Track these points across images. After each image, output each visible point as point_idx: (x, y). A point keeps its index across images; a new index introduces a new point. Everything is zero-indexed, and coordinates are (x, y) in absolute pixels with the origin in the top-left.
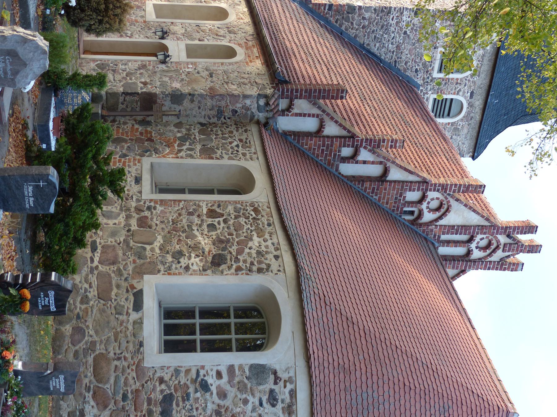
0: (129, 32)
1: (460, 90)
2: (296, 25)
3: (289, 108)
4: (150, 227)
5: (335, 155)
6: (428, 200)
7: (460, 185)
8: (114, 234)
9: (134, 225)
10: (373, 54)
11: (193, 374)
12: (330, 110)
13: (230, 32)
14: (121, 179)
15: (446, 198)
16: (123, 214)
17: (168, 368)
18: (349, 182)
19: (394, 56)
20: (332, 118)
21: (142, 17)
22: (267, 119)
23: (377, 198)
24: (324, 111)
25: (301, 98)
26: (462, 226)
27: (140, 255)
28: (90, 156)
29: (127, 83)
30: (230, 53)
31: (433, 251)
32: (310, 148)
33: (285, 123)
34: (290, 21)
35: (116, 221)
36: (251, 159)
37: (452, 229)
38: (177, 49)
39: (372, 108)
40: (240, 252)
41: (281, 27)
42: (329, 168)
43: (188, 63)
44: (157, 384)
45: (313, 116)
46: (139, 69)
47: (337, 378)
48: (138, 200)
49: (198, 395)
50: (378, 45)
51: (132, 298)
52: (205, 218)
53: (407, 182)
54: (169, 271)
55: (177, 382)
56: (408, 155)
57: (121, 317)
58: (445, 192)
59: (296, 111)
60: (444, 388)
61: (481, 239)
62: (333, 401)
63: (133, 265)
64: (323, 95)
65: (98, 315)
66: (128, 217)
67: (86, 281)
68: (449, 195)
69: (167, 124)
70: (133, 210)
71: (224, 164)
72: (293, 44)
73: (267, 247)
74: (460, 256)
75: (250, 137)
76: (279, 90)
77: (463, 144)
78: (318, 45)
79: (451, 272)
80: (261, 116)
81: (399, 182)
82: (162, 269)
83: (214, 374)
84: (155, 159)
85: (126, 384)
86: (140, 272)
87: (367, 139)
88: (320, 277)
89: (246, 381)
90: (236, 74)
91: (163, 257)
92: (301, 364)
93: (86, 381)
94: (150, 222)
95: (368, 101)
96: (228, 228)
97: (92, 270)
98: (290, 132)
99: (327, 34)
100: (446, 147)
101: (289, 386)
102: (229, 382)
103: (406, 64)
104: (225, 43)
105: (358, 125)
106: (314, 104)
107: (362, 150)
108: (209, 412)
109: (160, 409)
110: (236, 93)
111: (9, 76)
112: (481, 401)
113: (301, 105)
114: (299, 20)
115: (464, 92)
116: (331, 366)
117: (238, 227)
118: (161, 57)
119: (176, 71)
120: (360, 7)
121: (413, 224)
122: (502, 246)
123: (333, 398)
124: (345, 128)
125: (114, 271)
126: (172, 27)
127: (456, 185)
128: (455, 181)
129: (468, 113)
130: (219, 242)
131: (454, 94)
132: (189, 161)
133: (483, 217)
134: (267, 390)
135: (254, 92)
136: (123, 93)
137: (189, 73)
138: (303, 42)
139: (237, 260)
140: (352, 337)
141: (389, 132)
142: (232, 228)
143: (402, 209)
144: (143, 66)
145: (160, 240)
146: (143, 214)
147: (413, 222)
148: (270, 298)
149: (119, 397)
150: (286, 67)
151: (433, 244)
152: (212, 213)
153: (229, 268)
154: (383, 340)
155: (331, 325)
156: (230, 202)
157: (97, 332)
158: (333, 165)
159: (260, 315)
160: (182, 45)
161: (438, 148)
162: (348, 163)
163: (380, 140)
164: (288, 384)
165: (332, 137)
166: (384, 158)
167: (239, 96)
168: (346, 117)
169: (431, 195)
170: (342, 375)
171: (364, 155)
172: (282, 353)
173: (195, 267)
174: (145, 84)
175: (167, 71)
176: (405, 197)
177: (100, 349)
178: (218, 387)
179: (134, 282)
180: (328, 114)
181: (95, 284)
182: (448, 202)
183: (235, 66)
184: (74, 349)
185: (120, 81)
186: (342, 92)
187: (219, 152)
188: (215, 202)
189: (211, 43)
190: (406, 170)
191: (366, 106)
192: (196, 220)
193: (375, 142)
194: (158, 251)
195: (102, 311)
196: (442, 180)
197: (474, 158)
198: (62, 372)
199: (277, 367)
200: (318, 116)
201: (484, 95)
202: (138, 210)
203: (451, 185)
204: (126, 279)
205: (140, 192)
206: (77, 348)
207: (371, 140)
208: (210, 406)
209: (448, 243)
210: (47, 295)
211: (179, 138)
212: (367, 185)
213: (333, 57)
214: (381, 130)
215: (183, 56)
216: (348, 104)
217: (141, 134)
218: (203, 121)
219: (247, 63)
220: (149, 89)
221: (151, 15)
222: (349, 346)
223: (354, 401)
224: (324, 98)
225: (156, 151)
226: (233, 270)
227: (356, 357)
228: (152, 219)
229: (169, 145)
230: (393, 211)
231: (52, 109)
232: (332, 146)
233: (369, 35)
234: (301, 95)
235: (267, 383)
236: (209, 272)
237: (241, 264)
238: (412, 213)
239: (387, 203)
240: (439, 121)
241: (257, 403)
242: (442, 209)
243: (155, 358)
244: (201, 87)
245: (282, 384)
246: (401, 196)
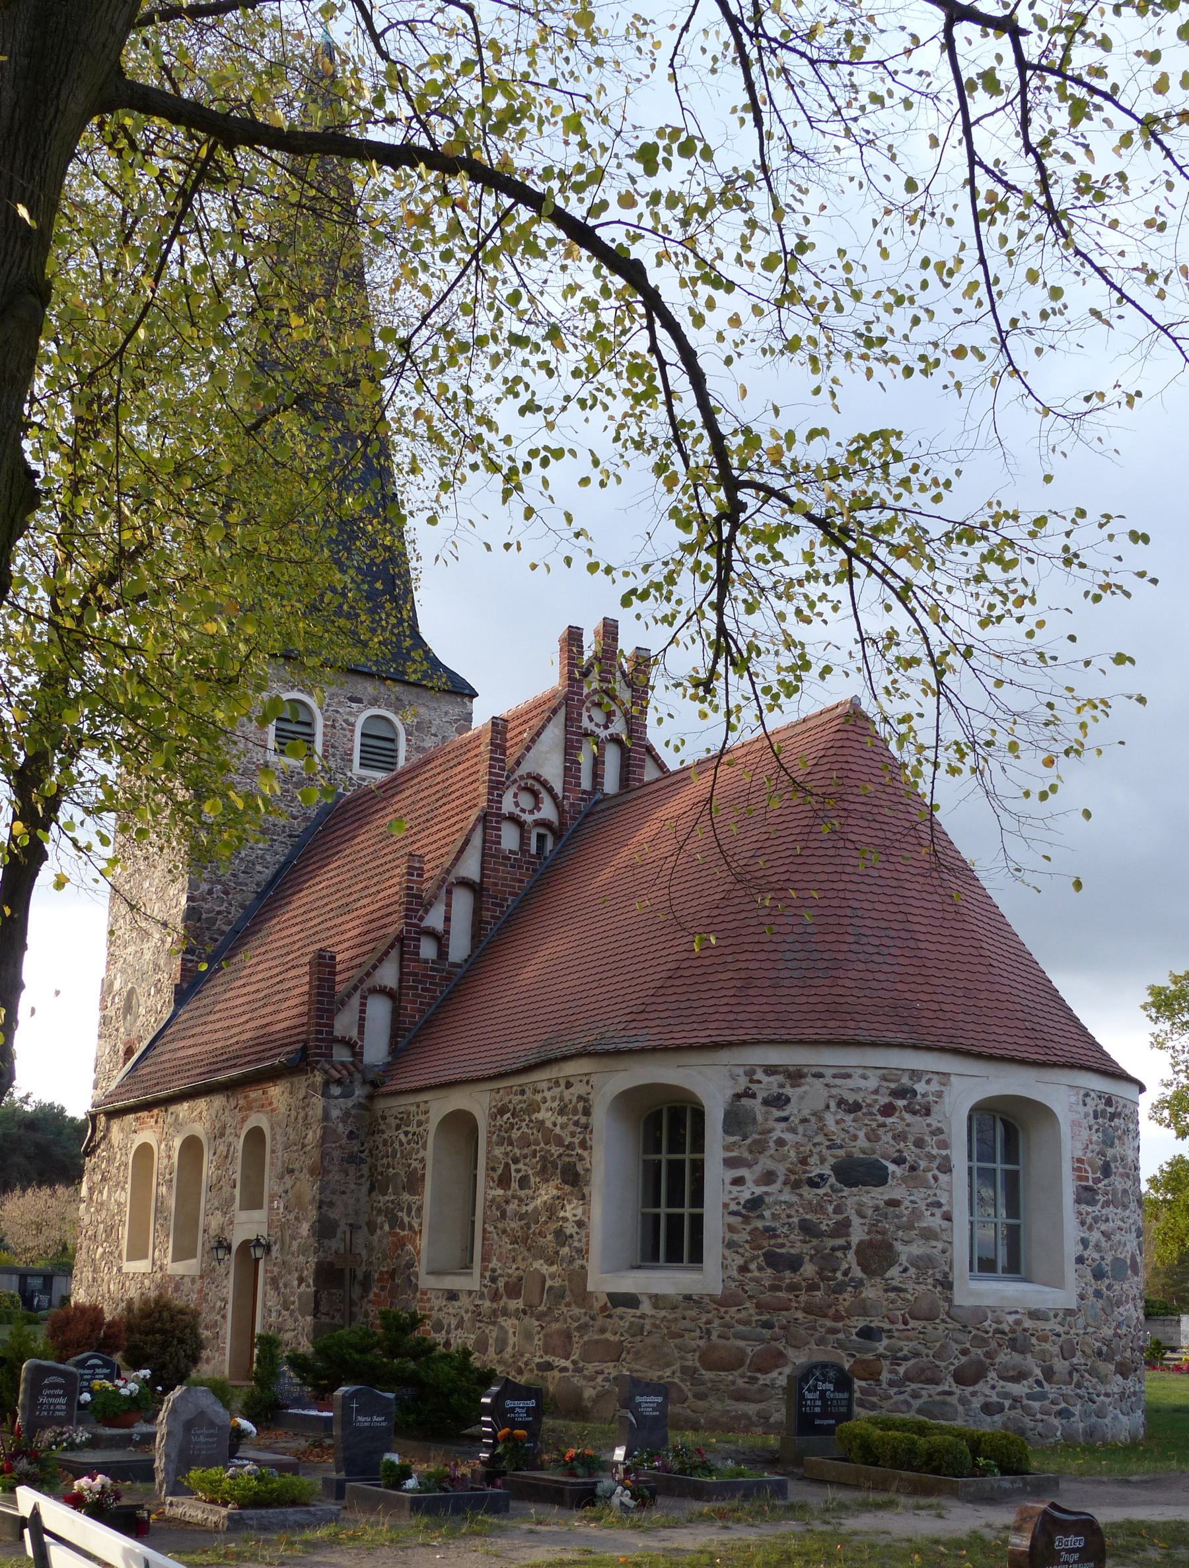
0: (219, 1304)
1: (346, 721)
2: (218, 1016)
3: (350, 1044)
4: (520, 1279)
5: (432, 969)
6: (517, 811)
7: (491, 759)
8: (528, 1336)
9: (517, 1304)
10: (276, 875)
11: (735, 1220)
12: (357, 973)
13: (222, 1135)
14: (397, 1317)
15: (515, 781)
16: (501, 1320)
17: (724, 1258)
18: (482, 946)
19: (281, 839)
20: (368, 974)
21: (193, 1281)
22: (364, 1082)
23: (510, 898)
24: (355, 988)
25: (332, 1026)
26: (566, 754)
27: (558, 1295)
28: (356, 1356)
29: (299, 1309)
30: (256, 1135)
31: (613, 803)
32: (419, 1010)
33: (376, 1050)
34: (210, 1027)
35: (511, 1331)
36: (426, 1112)
37: (571, 770)
38: (248, 1225)
39: (364, 893)
40: (559, 1141)
41: (219, 1045)
42: (455, 979)
43: (271, 1209)
44: (749, 1275)
45: (363, 1005)
46: (277, 1288)
47: (755, 1000)
48: (482, 1296)
49: (767, 1214)
50: (259, 868)
51: (620, 1310)
52: (510, 1193)
53: (484, 849)
54: (583, 1253)
55: (747, 1246)
56: (435, 847)
57: (647, 1327)
58: (503, 783)
59: (354, 1034)
60: (796, 823)
61: (591, 719)
62: (788, 1008)
63: (573, 1306)
64: (326, 987)
65: (643, 1361)
66: (505, 1312)
67: (592, 1379)
68: (508, 778)
69: (369, 1247)
70: (495, 1306)
71: (430, 1155)
72: (248, 1026)
73: (553, 1099)
74: (622, 755)
75: (394, 1111)
76: (318, 1062)
77: (446, 713)
78: (254, 979)
79: (650, 773)
80: (360, 1092)
81: (483, 862)
82: (580, 1262)
83: (736, 1188)
84: (421, 1268)
85: (746, 1323)
86: (583, 1297)
87: (406, 916)
88: (604, 1017)
89: (749, 1141)
90: (289, 1130)
91: (562, 1260)
92: (724, 1056)
93: (740, 1382)
94: (514, 1279)
95: (340, 909)
96: (525, 1157)
97: (578, 1370)
98: (391, 1044)
99: (235, 960)
100: (440, 761)
101: (759, 1075)
102: (749, 1166)
103: (295, 818)
104: (239, 1144)
105: (385, 926)
106: (343, 1003)
107: (426, 923)
108: (795, 1199)
109: (788, 1273)
110: (319, 1133)
111: (215, 1431)
112: (825, 760)
113: (344, 1024)
114: (208, 1010)
115: (350, 713)
116: (736, 1009)
117: (525, 1142)
118: (259, 1253)
119: (282, 1227)
120: (189, 899)
121: (561, 836)
122: (605, 686)
123: (784, 1008)
124: (386, 953)
125: (581, 1337)
126: (212, 1232)
127: (491, 766)
128: (483, 767)
129: (388, 705)
130: (545, 1172)
131: (352, 731)
132: (426, 1212)
133: (549, 719)
134: (764, 1109)
135: (318, 1102)
136: (315, 1316)
137: (286, 1208)
138: (246, 1008)
139: (570, 1146)
140: (698, 971)
141: (396, 880)
142: (525, 1151)
143: (532, 856)
144: (274, 1282)
145: (538, 1264)
146: (501, 1290)
147: (557, 836)
148: (630, 1100)
149: (767, 1333)
150: (282, 1046)
151: (596, 803)
152: (504, 1181)
153: (581, 1159)
154: (709, 921)
155: (675, 1006)
156: (489, 1152)
157: (668, 1365)
158: (449, 973)
159: (657, 1115)
160: (242, 1216)
161: (439, 778)
162: (447, 946)
163: (408, 895)
164: (755, 1077)
165: (402, 973)
166: (439, 887)
167: (324, 1128)
168: (371, 946)
169: (508, 805)
170: (752, 992)
171: (434, 919)
172: (710, 1083)
173: (579, 1211)
174: (301, 1280)
175: (283, 1243)
176: (511, 852)
177: (692, 1361)
178: (758, 1183)
179: (597, 1305)
180: (361, 981)
181: (597, 1366)
182: (521, 777)
183: (278, 1130)
184: (691, 1399)
185: (296, 1321)
186: (323, 957)
187: (415, 1164)
188: (487, 1176)
189: (239, 1168)
190: (462, 850)
191: (359, 904)
192: (513, 1206)
193: (410, 903)
194: (554, 1268)
195: (638, 1356)
196: (483, 789)
197: (473, 695)
198: (632, 1399)
199: (730, 1093)
200: (364, 997)
201: (360, 680)
202: (495, 1297)
203: (491, 774)
204: (593, 1318)
205: (470, 1293)
206: (690, 1395)
207: (407, 909)
208: (786, 1196)
209: (597, 776)
210: (512, 1410)
211: (392, 1227)
212: (487, 915)
213: (275, 954)
214: (393, 887)
215: (260, 1215)
216: (352, 938)
217: (383, 1288)
218: (365, 1188)
219: (273, 1110)
220: (309, 1273)
221: (189, 1267)
222: (711, 978)
223: (795, 974)
224: (332, 988)
225: (410, 1265)
226: (585, 1154)
227: (730, 967)
228: (509, 1276)
229: (401, 1244)
230: (534, 871)
231: (306, 1412)
232: (416, 974)
233: (241, 884)
234: (326, 1025)
235: (752, 1110)
236: (586, 1190)
237: (576, 1141)
238: (541, 838)
239: (521, 881)
240: (401, 762)
241: (783, 1125)
242: (535, 787)
243: (708, 1277)
244: (309, 1188)
245: (754, 1087)
246: (509, 859)
